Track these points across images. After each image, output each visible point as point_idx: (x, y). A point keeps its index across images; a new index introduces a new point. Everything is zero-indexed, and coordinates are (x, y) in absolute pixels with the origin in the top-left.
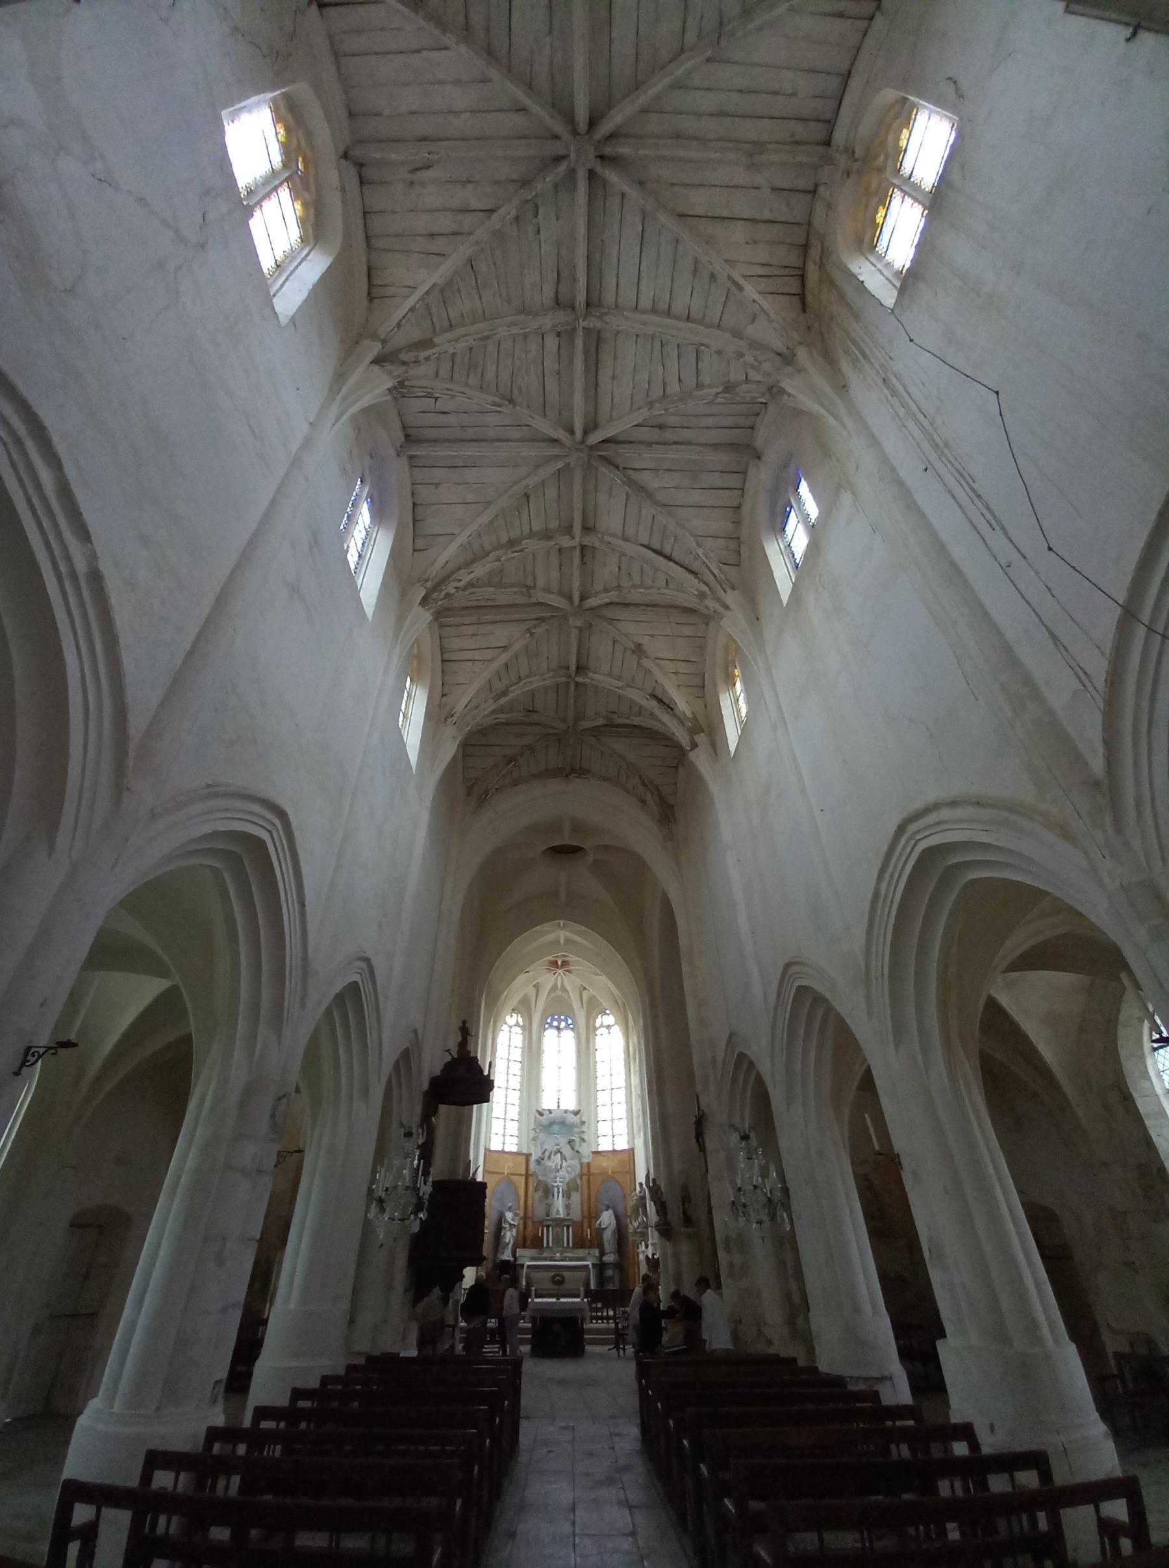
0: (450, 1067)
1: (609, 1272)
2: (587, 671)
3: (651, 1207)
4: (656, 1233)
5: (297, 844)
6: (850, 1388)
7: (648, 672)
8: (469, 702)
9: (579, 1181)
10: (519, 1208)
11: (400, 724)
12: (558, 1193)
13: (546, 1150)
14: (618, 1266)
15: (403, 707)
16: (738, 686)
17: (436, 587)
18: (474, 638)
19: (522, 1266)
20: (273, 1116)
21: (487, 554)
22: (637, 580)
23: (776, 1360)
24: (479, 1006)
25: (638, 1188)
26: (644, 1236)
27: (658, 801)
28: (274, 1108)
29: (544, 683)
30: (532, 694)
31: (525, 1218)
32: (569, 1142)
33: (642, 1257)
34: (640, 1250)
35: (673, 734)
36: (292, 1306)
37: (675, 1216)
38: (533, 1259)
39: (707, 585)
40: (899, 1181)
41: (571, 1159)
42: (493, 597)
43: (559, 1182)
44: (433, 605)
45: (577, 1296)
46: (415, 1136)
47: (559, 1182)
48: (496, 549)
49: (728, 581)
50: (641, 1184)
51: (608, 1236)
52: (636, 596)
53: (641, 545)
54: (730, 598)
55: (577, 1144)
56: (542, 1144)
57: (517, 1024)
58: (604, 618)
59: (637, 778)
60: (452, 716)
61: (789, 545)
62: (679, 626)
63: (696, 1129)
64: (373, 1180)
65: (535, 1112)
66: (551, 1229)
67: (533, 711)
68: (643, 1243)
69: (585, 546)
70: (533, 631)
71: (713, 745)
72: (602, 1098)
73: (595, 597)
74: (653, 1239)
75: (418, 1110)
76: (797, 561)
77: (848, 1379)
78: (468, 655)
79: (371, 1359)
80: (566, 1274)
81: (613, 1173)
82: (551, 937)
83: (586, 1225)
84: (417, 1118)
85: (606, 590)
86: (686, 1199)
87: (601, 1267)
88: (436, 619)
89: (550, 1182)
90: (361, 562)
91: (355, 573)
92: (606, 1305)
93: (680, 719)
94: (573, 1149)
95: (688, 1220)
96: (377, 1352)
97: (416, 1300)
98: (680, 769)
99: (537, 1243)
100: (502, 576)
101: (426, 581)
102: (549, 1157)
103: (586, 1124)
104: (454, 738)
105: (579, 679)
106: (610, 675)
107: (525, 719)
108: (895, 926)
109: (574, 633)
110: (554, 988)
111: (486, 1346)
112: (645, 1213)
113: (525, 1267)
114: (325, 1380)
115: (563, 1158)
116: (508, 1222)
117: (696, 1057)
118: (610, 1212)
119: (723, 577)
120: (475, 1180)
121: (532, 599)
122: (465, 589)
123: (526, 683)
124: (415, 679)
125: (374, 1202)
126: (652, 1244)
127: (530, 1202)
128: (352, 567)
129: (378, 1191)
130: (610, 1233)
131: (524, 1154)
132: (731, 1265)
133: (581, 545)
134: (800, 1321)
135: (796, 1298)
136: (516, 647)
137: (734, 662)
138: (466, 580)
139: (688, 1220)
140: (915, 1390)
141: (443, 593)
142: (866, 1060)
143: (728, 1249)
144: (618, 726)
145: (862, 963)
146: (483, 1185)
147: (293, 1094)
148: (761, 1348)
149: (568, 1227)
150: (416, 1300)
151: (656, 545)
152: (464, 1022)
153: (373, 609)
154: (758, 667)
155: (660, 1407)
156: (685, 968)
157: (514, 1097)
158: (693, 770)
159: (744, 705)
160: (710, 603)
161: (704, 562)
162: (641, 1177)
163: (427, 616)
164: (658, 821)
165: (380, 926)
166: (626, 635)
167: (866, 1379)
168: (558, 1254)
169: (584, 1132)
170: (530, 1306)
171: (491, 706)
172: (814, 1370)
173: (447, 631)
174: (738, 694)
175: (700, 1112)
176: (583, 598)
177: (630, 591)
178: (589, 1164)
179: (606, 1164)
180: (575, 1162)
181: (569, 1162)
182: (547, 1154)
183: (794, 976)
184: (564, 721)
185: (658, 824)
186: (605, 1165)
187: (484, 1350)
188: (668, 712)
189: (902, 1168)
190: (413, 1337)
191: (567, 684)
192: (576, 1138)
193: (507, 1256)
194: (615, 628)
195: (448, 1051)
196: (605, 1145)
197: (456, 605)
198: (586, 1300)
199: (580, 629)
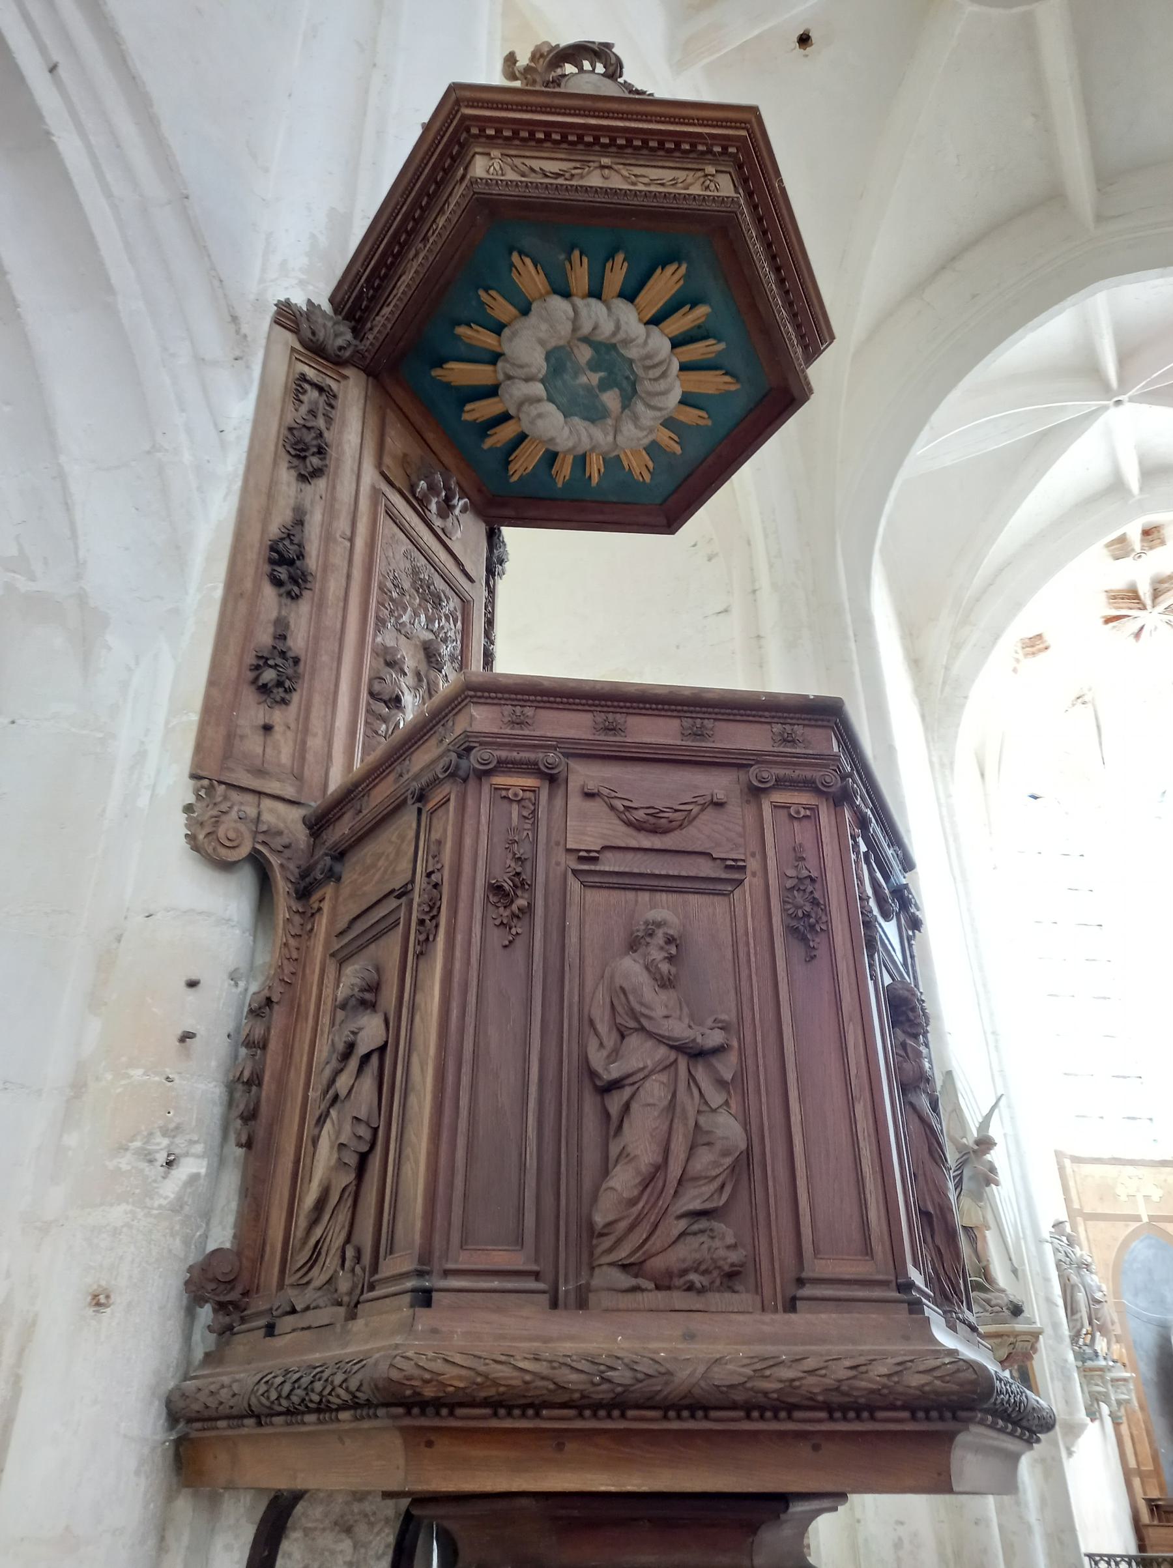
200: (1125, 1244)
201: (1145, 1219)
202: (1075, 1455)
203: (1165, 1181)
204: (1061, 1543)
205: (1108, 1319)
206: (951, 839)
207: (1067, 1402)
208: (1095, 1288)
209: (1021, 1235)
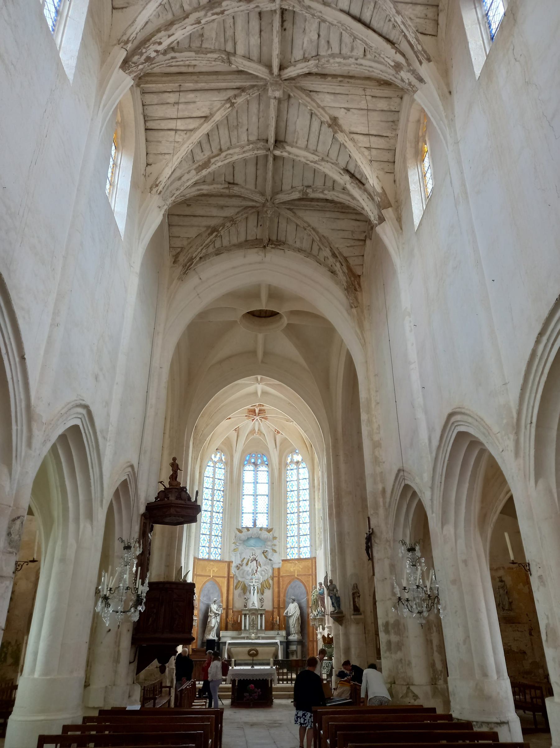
0: (163, 495)
1: (293, 647)
2: (285, 145)
3: (328, 601)
4: (331, 620)
5: (13, 302)
6: (476, 729)
7: (342, 146)
8: (172, 173)
9: (271, 582)
10: (222, 602)
11: (107, 191)
14: (301, 643)
15: (109, 175)
16: (427, 162)
17: (137, 50)
18: (176, 106)
19: (225, 643)
20: (9, 534)
21: (187, 17)
22: (336, 50)
23: (420, 709)
24: (188, 447)
25: (318, 587)
26: (322, 621)
27: (346, 271)
28: (9, 528)
29: (244, 155)
30: (233, 165)
31: (227, 609)
33: (319, 636)
34: (318, 631)
35: (363, 209)
36: (36, 675)
37: (347, 606)
38: (233, 638)
39: (404, 55)
40: (528, 583)
41: (265, 565)
42: (194, 63)
43: (255, 581)
44: (133, 69)
45: (268, 664)
46: (132, 549)
47: (255, 581)
48: (196, 10)
49: (425, 52)
50: (321, 584)
51: (293, 622)
52: (333, 67)
53: (342, 11)
54: (425, 70)
55: (270, 554)
56: (241, 554)
58: (303, 90)
59: (328, 250)
60: (157, 186)
61: (487, 14)
62: (374, 100)
63: (367, 543)
64: (99, 582)
65: (236, 530)
66: (248, 616)
67: (233, 184)
68: (321, 626)
69: (286, 10)
70: (233, 101)
71: (399, 219)
72: (292, 518)
73: (295, 66)
74: (329, 623)
75: (137, 528)
76: (494, 32)
77: (475, 723)
78: (172, 124)
79: (102, 712)
80: (259, 649)
81: (297, 575)
82: (251, 389)
83: (276, 614)
84: (136, 534)
85: (305, 59)
86: (356, 594)
87: (287, 644)
88: (138, 85)
89: (247, 582)
90: (59, 18)
91: (53, 30)
92: (290, 670)
93: (370, 194)
94: (266, 557)
95: (356, 610)
96: (108, 707)
97: (139, 669)
98: (368, 242)
99: (237, 627)
100: (202, 41)
101: (127, 42)
102: (247, 564)
103: (278, 539)
104: (160, 207)
105: (277, 153)
106: (306, 148)
107: (227, 191)
108: (546, 383)
109: (273, 103)
110: (253, 432)
111: (195, 701)
112: (323, 605)
114: (66, 728)
115: (258, 564)
117: (369, 486)
118: (296, 604)
119: (420, 48)
120: (186, 581)
121: (233, 66)
122: (165, 53)
123: (227, 155)
124: (121, 148)
125: (100, 599)
126: (328, 627)
127: (231, 598)
128: (50, 23)
129: (103, 591)
131: (226, 562)
132: (389, 643)
133: (281, 8)
134: (441, 682)
135: (439, 666)
136: (218, 117)
137: (424, 136)
138: (166, 43)
139: (356, 610)
140: (525, 731)
141: (144, 57)
142: (510, 490)
143: (387, 632)
144: (312, 200)
145: (515, 415)
146: (192, 585)
147: (26, 516)
148: (410, 701)
149: (261, 615)
150: (139, 669)
151: (355, 11)
152: (174, 459)
153: (73, 71)
154: (447, 143)
155: (329, 742)
156: (364, 417)
157: (218, 518)
158: (379, 244)
159: (431, 180)
160: (405, 75)
161: (403, 31)
162: (321, 579)
163: (128, 81)
164: (346, 290)
165: (96, 378)
166: (323, 108)
167: (488, 723)
168: (253, 635)
169: (275, 545)
170: (229, 672)
171: (194, 177)
172: (450, 717)
173: (149, 99)
174: (426, 169)
175: (371, 530)
176: (282, 68)
177: (328, 61)
178: (279, 569)
179: (292, 568)
180: (269, 568)
181: (263, 567)
183: (456, 424)
184: (263, 194)
185: (346, 292)
186: (292, 570)
187: (193, 704)
188: (360, 188)
189: (531, 574)
190: (137, 694)
191: (266, 156)
192: (269, 549)
193: (212, 636)
194: (313, 100)
195: (161, 482)
196: (293, 554)
197: (157, 70)
198: (274, 667)
199: (280, 101)
200: (205, 583)
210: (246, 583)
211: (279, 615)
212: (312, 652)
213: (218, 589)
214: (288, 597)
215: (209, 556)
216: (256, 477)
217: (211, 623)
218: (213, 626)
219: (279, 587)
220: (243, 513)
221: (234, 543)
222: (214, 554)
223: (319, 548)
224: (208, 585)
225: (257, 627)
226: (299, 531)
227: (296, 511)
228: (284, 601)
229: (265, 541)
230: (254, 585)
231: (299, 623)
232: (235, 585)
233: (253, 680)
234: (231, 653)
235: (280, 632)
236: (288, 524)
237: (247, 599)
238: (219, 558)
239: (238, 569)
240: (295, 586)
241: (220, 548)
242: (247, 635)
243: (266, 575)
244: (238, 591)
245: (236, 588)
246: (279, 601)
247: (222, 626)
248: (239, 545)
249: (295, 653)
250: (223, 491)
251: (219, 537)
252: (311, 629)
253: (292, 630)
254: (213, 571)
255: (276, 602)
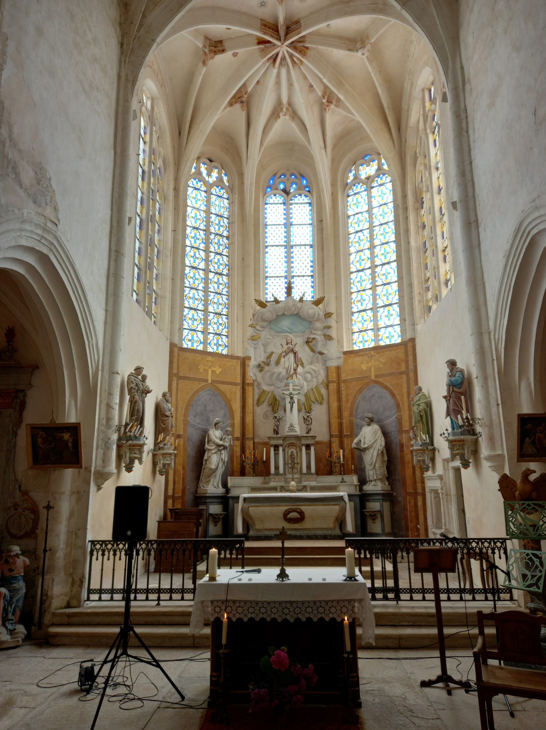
1: (374, 506)
9: (323, 391)
10: (233, 426)
12: (292, 404)
13: (272, 353)
14: (388, 497)
19: (237, 498)
32: (307, 342)
38: (254, 489)
41: (311, 364)
56: (265, 346)
57: (219, 183)
65: (254, 301)
66: (281, 449)
80: (306, 509)
81: (376, 376)
89: (278, 393)
94: (313, 350)
102: (278, 363)
103: (334, 316)
113: (241, 501)
115: (298, 362)
116: (214, 443)
118: (375, 427)
127: (249, 419)
130: (375, 454)
131: (237, 358)
149: (308, 447)
178: (338, 368)
180: (318, 368)
181: (308, 367)
182: (274, 359)
186: (364, 367)
200: (197, 392)
201: (210, 381)
202: (102, 489)
203: (225, 364)
204: (76, 535)
205: (170, 425)
206: (120, 129)
207: (103, 461)
208: (166, 409)
209: (100, 368)
210: (276, 393)
211: (342, 447)
212: (414, 514)
213: (223, 403)
214: (359, 416)
215: (205, 347)
216: (288, 215)
217: (210, 463)
218: (213, 467)
219: (339, 400)
220: (267, 277)
221: (251, 326)
222: (215, 344)
223: (423, 320)
224: (205, 396)
225: (301, 468)
226: (375, 299)
227: (368, 265)
228: (351, 423)
229: (309, 321)
230: (291, 394)
231: (383, 461)
232: (256, 397)
233: (286, 621)
234: (251, 517)
235: (347, 478)
236: (352, 291)
237: (278, 420)
238: (225, 352)
239: (261, 371)
240: (373, 396)
241: (227, 336)
242: (282, 484)
243: (315, 379)
244: (264, 408)
245: (259, 403)
246: (341, 425)
247: (235, 469)
248: (260, 329)
249: (379, 516)
250: (227, 238)
251: (224, 317)
252: (409, 472)
253: (370, 473)
254: (213, 372)
255: (335, 426)
